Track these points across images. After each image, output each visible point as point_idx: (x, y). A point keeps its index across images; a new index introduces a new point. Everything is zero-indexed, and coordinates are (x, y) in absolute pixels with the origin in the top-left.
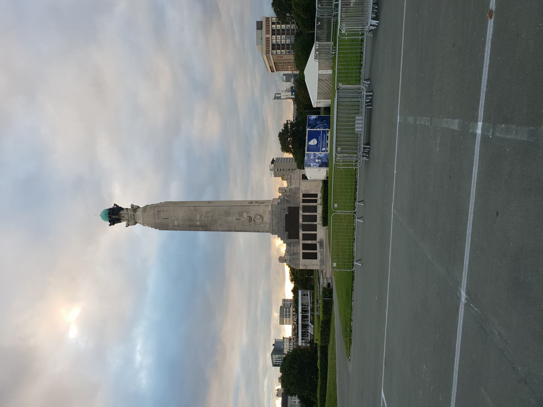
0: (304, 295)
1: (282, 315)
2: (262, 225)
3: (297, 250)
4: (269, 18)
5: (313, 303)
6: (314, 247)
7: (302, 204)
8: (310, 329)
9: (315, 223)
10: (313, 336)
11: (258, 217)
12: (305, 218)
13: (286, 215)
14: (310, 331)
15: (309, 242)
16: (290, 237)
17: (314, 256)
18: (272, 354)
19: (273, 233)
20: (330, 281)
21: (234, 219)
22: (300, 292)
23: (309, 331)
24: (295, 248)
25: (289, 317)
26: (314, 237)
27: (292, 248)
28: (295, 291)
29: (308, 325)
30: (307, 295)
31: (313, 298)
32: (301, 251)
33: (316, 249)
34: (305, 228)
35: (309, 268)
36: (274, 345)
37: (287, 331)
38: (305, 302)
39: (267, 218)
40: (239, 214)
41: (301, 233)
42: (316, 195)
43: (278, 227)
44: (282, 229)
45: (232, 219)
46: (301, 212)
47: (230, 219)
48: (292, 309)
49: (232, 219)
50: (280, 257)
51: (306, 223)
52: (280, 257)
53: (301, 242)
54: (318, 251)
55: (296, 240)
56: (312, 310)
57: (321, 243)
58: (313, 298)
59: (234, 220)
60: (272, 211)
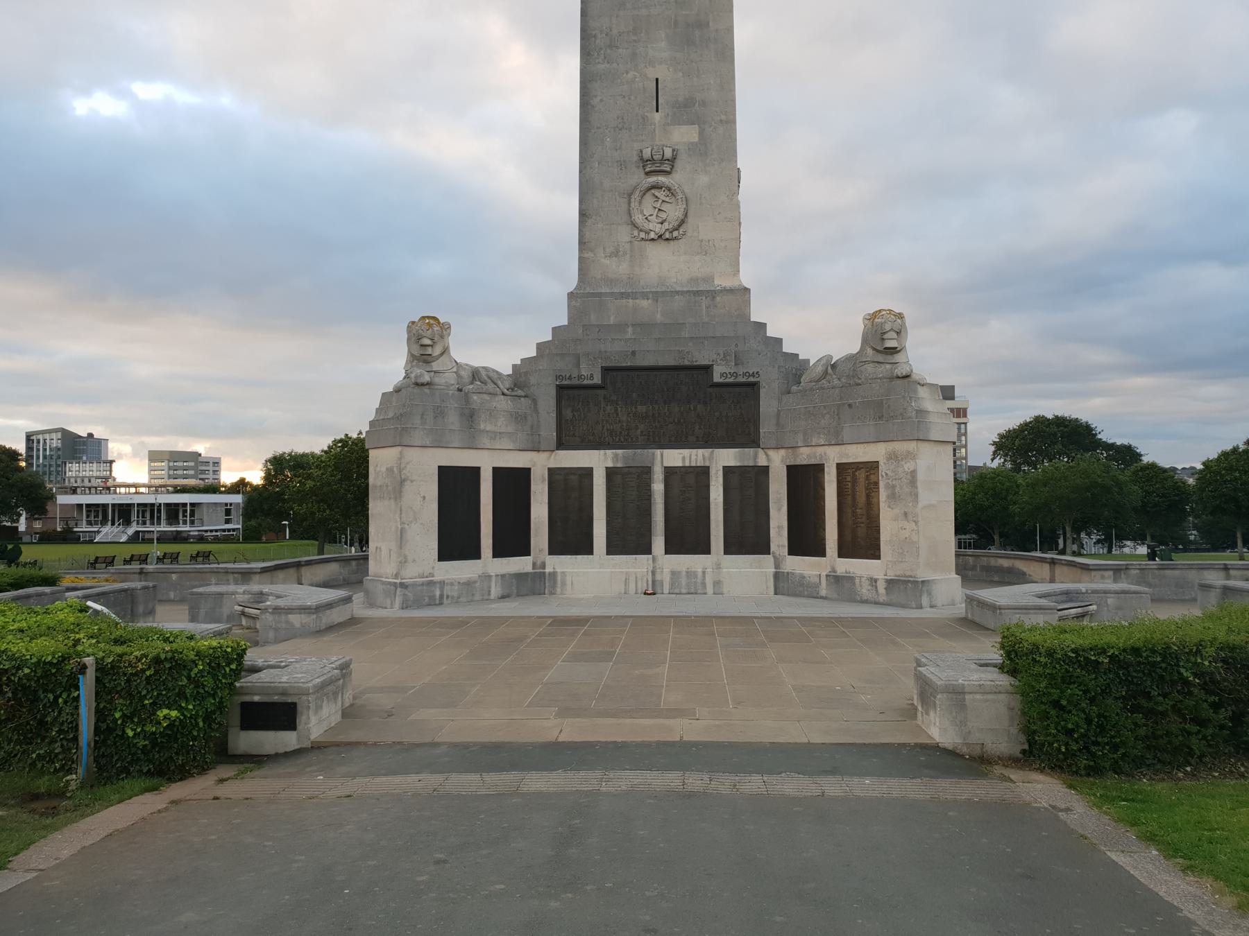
0: (228, 512)
1: (175, 457)
2: (623, 235)
3: (494, 436)
4: (965, 416)
5: (201, 539)
6: (513, 540)
7: (777, 462)
8: (115, 529)
9: (658, 543)
10: (91, 542)
11: (673, 212)
12: (690, 484)
13: (707, 369)
14: (107, 532)
15: (539, 511)
16: (567, 392)
17: (456, 541)
18: (64, 431)
19: (580, 300)
20: (318, 722)
21: (662, 72)
22: (238, 499)
23: (107, 529)
24: (502, 424)
25: (170, 477)
26: (571, 537)
27: (503, 403)
28: (240, 486)
29: (128, 523)
30: (227, 521)
31: (217, 540)
32: (486, 461)
33: (499, 552)
34: (628, 488)
35: (376, 507)
36: (91, 435)
37: (131, 472)
38: (204, 513)
39: (665, 265)
40: (688, 103)
41: (598, 461)
42: (871, 549)
43: (621, 327)
44: (617, 350)
45: (660, 62)
46: (727, 457)
47: (660, 47)
48: (192, 482)
49: (660, 62)
50: (445, 328)
51: (658, 487)
52: (445, 328)
53: (540, 464)
54: (490, 566)
55: (549, 431)
56: (179, 538)
57: (535, 584)
58: (217, 540)
59: (652, 73)
60: (712, 294)
